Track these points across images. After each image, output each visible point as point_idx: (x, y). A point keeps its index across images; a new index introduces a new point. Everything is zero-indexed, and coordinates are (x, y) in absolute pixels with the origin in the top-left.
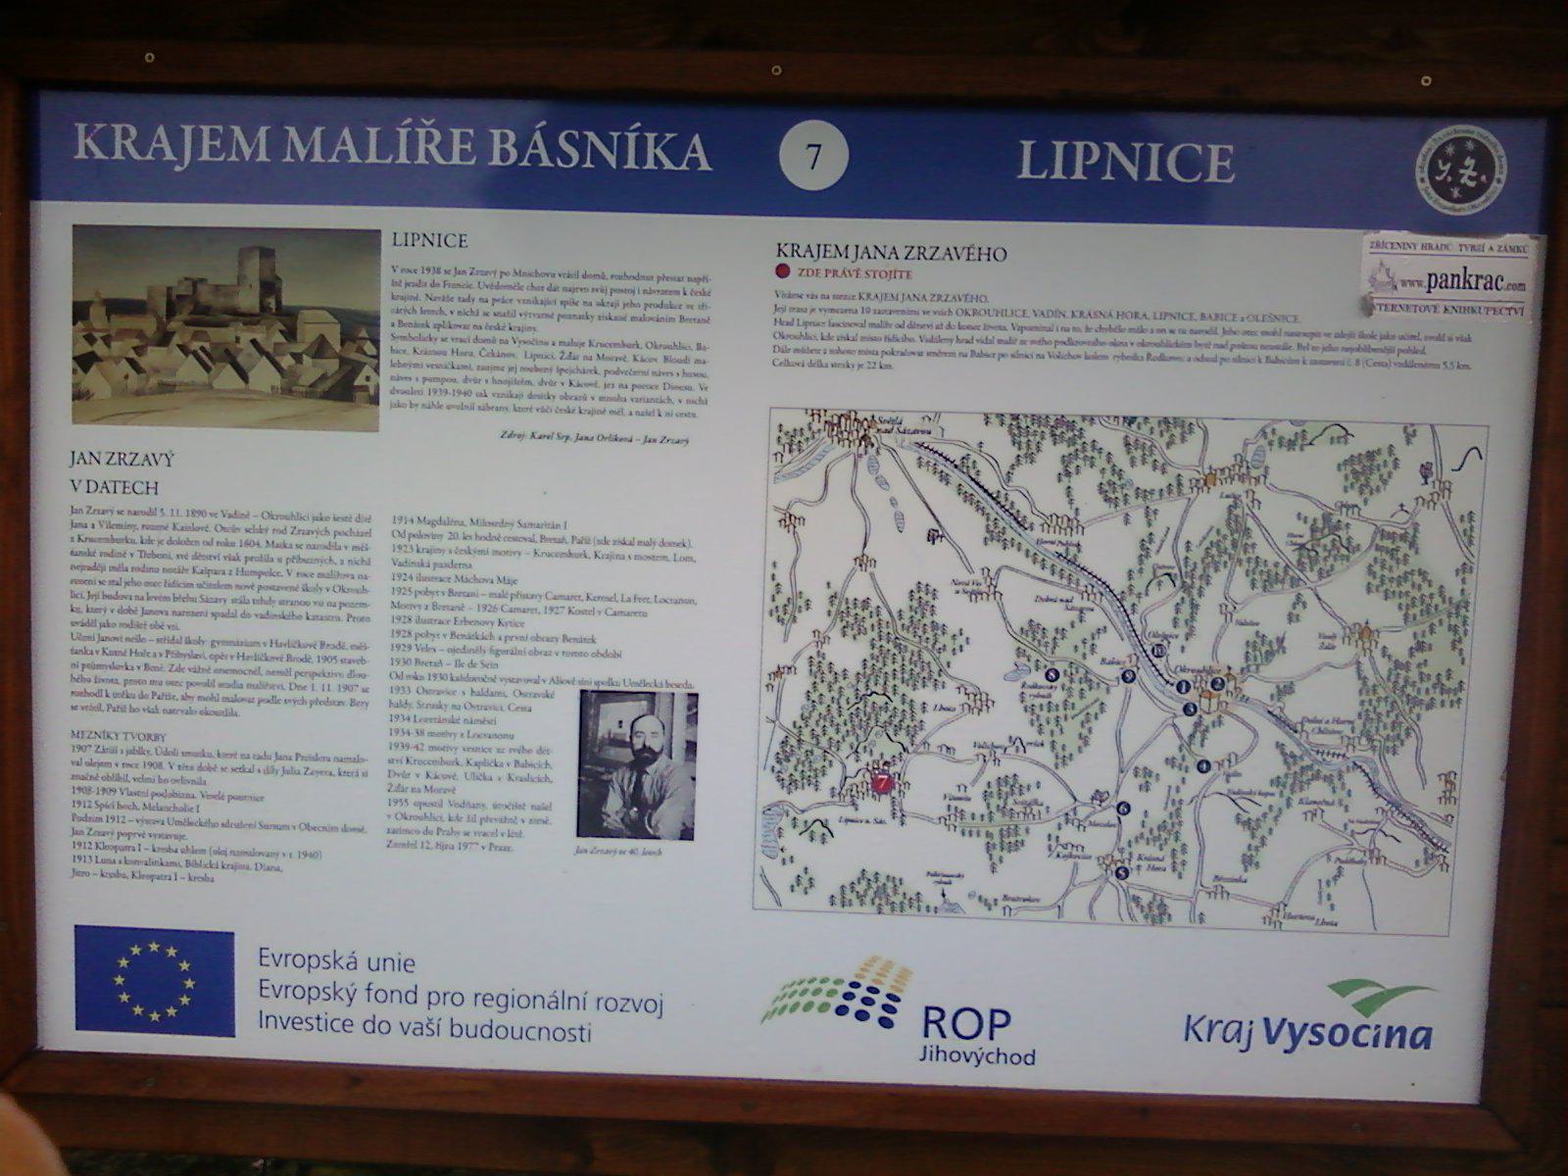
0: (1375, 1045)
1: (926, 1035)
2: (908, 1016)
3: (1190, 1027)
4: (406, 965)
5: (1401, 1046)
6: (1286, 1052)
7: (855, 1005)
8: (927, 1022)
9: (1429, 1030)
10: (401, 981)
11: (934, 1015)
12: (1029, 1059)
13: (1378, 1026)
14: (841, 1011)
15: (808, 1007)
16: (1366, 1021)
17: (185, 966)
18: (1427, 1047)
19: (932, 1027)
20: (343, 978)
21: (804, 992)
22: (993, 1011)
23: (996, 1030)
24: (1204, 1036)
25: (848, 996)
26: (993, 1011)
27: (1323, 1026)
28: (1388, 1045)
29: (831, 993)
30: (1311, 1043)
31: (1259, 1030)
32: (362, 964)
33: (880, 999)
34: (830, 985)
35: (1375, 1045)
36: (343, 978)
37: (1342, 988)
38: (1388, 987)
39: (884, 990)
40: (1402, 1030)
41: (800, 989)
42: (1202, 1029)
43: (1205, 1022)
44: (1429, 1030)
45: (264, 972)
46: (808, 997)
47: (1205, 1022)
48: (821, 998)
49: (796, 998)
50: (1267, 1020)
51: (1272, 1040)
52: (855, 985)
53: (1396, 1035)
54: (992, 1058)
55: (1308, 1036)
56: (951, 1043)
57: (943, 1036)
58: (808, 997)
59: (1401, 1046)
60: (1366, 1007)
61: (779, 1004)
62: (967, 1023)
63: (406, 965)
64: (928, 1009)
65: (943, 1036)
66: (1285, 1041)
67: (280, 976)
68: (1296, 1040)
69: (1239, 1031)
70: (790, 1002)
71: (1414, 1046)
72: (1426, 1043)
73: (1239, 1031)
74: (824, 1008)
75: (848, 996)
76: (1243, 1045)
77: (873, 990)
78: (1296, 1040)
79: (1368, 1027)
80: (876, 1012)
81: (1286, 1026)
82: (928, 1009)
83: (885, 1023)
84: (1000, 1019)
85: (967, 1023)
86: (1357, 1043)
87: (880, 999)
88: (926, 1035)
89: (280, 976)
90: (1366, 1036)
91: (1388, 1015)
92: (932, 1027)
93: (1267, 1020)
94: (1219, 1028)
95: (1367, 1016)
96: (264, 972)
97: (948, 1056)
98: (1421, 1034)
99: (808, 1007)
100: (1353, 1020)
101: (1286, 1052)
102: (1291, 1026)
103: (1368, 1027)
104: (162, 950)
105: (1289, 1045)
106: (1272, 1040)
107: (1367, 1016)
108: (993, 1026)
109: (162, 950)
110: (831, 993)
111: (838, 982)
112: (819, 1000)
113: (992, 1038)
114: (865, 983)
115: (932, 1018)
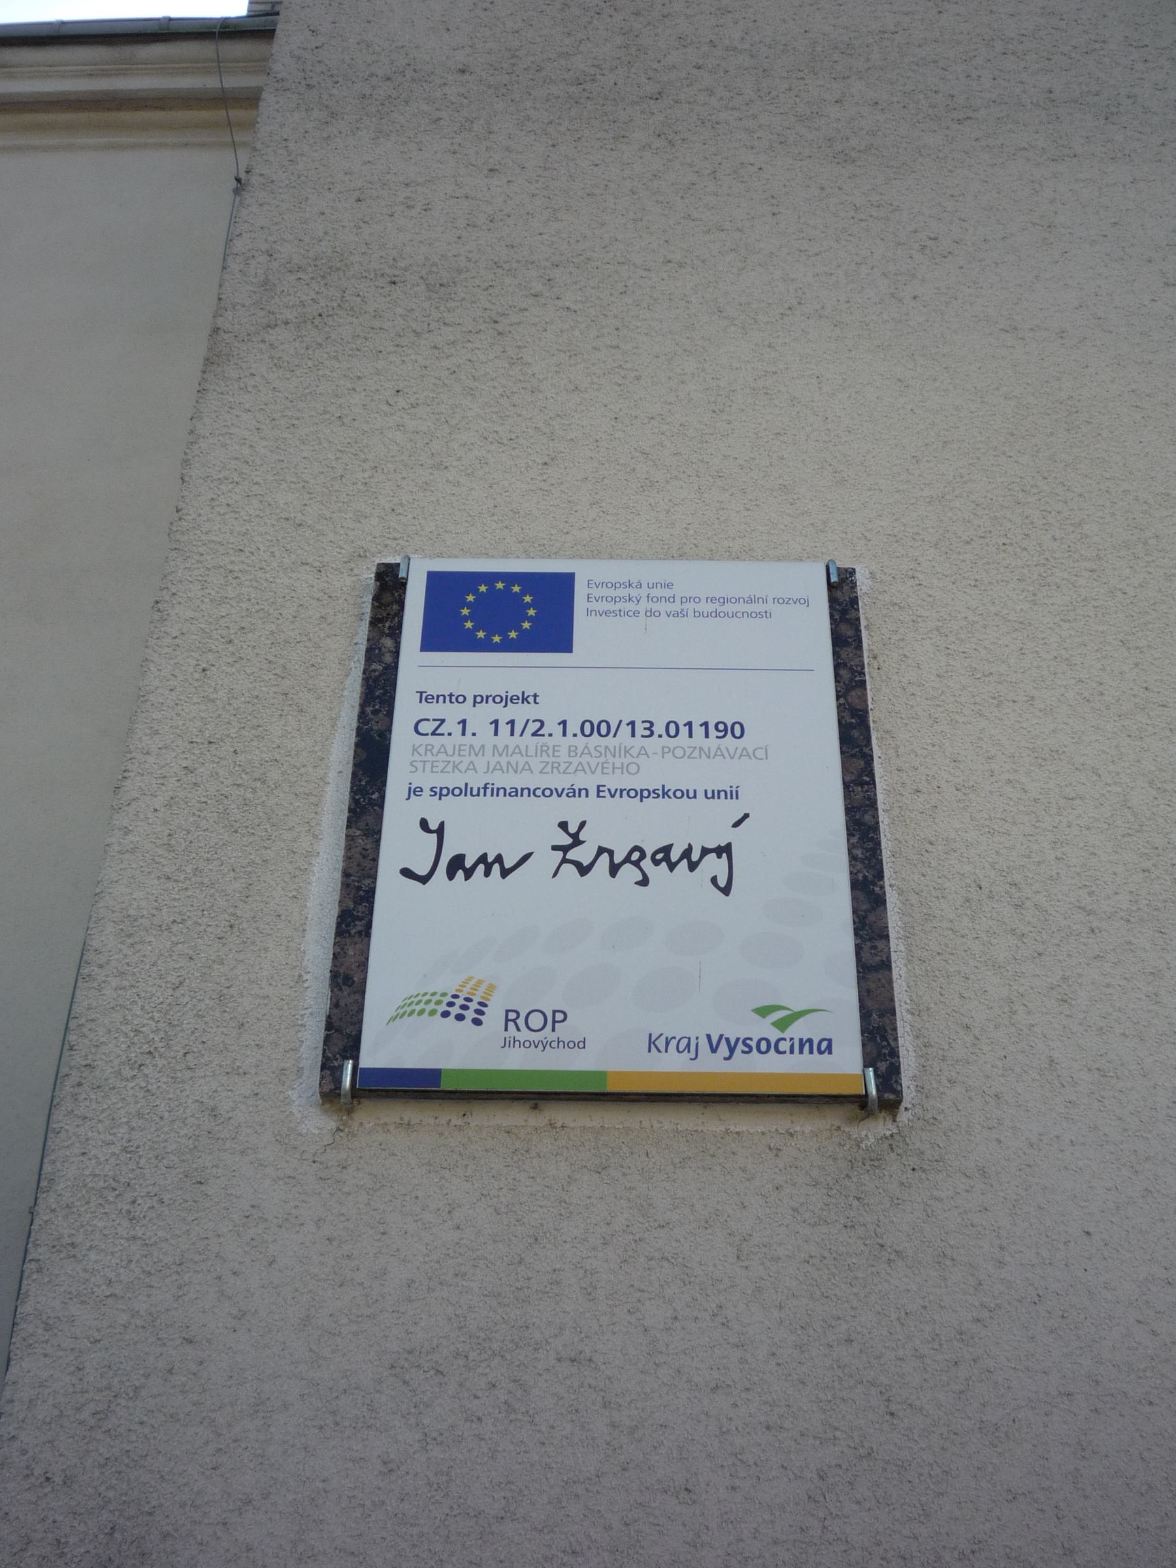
0: (792, 1052)
1: (506, 1029)
2: (494, 1017)
3: (652, 1043)
4: (669, 585)
5: (811, 1052)
6: (725, 1059)
7: (455, 1010)
8: (507, 1020)
9: (830, 1041)
10: (667, 593)
11: (512, 1016)
12: (582, 1044)
13: (791, 1039)
14: (446, 1014)
15: (422, 1012)
16: (782, 1036)
17: (481, 634)
18: (830, 1053)
19: (511, 1024)
20: (634, 592)
21: (419, 1002)
22: (554, 1012)
23: (557, 1025)
24: (663, 1049)
25: (451, 1004)
26: (554, 1012)
27: (751, 1039)
28: (801, 1052)
29: (439, 1003)
30: (743, 1052)
31: (704, 1042)
32: (644, 585)
33: (473, 1006)
34: (437, 997)
35: (792, 1052)
36: (634, 592)
37: (763, 1012)
38: (796, 1010)
39: (476, 999)
40: (810, 1041)
41: (416, 1000)
42: (661, 1044)
43: (663, 1039)
44: (830, 1041)
45: (590, 591)
46: (422, 1006)
47: (663, 1039)
48: (432, 1006)
49: (413, 1007)
50: (709, 1037)
51: (714, 1050)
52: (455, 996)
53: (805, 1044)
54: (554, 1044)
55: (740, 1046)
56: (524, 1035)
57: (518, 1030)
58: (422, 1006)
59: (811, 1052)
60: (782, 1025)
61: (401, 1011)
62: (536, 1021)
63: (669, 585)
64: (507, 1011)
65: (518, 1030)
66: (723, 1050)
67: (597, 592)
68: (732, 1050)
69: (688, 1045)
70: (409, 1010)
71: (821, 1052)
72: (829, 1049)
73: (688, 1045)
74: (432, 1013)
75: (451, 1004)
76: (693, 1055)
77: (468, 1000)
78: (732, 1050)
79: (784, 1039)
80: (470, 1015)
81: (723, 1041)
82: (507, 1011)
83: (477, 1022)
84: (559, 1017)
85: (536, 1021)
86: (778, 1051)
87: (473, 1006)
88: (506, 1029)
89: (597, 592)
90: (784, 1046)
91: (798, 1031)
92: (511, 1024)
93: (709, 1037)
94: (673, 1043)
95: (783, 1031)
96: (590, 591)
97: (522, 1044)
98: (824, 1045)
99: (422, 1012)
100: (774, 1035)
101: (725, 1059)
102: (728, 1040)
103: (784, 1039)
104: (507, 588)
105: (727, 1054)
106: (714, 1050)
107: (783, 1031)
108: (554, 1022)
109: (507, 588)
110: (439, 1003)
111: (444, 995)
112: (429, 1008)
113: (553, 1030)
114: (462, 995)
115: (511, 1018)
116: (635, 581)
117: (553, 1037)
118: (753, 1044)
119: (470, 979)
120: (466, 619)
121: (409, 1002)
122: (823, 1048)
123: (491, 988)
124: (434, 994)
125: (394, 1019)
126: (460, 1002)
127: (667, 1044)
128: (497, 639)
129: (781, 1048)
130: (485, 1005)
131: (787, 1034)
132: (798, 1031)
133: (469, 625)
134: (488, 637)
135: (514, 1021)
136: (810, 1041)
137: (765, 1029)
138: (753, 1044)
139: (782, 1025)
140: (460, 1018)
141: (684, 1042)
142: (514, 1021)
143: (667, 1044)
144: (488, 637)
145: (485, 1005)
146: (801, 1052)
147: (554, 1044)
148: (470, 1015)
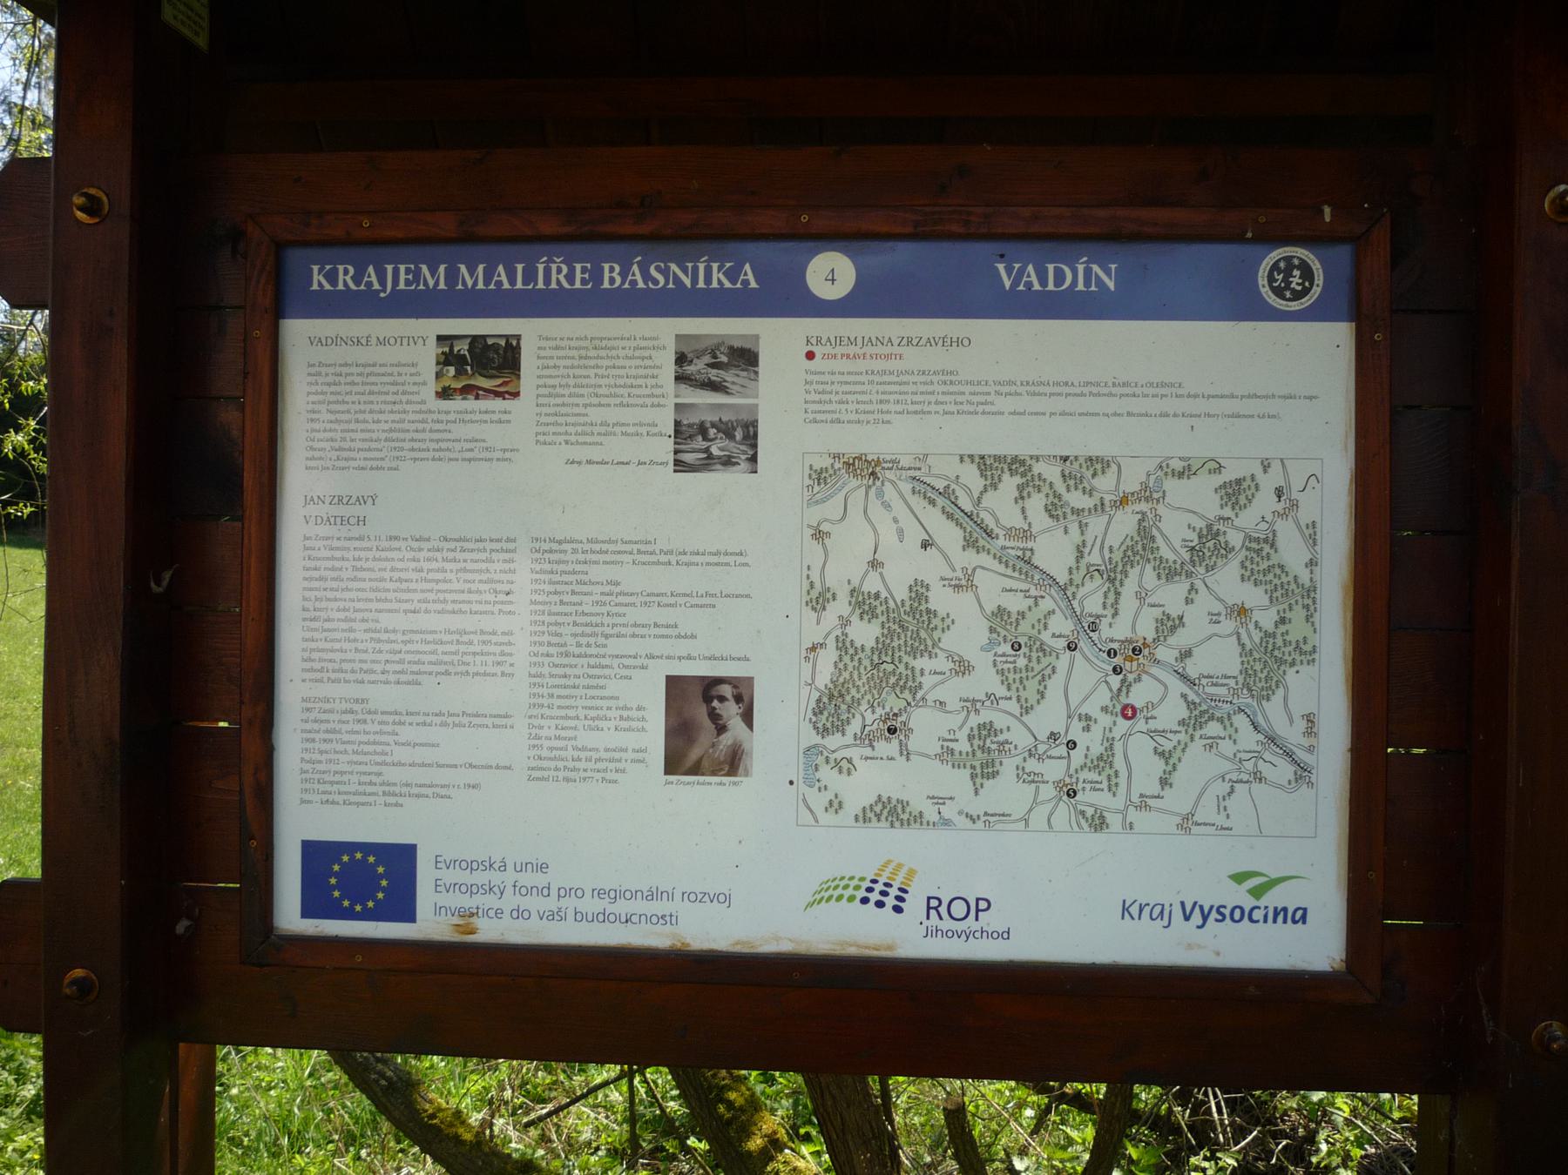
0: (1265, 921)
3: (1125, 909)
7: (875, 896)
8: (929, 908)
9: (1305, 910)
11: (934, 903)
14: (865, 901)
15: (839, 898)
16: (1256, 903)
17: (346, 903)
19: (933, 912)
21: (836, 887)
22: (978, 900)
24: (1136, 916)
25: (870, 890)
26: (978, 900)
28: (1275, 921)
29: (857, 888)
32: (510, 867)
33: (894, 892)
34: (855, 882)
35: (1265, 921)
36: (495, 877)
37: (1239, 878)
39: (896, 885)
40: (1285, 910)
42: (1134, 910)
44: (1305, 910)
45: (439, 873)
48: (850, 892)
49: (830, 892)
50: (1183, 904)
51: (1187, 918)
52: (874, 881)
54: (978, 935)
55: (1214, 915)
56: (947, 924)
59: (1285, 921)
60: (1257, 892)
61: (818, 897)
62: (959, 909)
64: (929, 899)
66: (1197, 918)
67: (450, 876)
68: (1205, 918)
69: (1162, 912)
70: (826, 895)
72: (1304, 919)
73: (1162, 912)
74: (851, 899)
75: (870, 890)
76: (1166, 922)
78: (1205, 918)
80: (890, 901)
81: (1197, 909)
82: (929, 899)
83: (898, 910)
84: (983, 905)
85: (959, 909)
87: (894, 892)
89: (450, 876)
90: (1257, 915)
91: (1273, 899)
92: (933, 912)
93: (1183, 904)
94: (1147, 910)
95: (1258, 898)
97: (945, 934)
99: (839, 898)
100: (1248, 902)
102: (1201, 908)
105: (1200, 922)
106: (1187, 918)
107: (1258, 898)
108: (978, 910)
110: (857, 888)
112: (847, 893)
116: (497, 858)
117: (975, 926)
118: (1227, 912)
119: (889, 862)
120: (333, 888)
121: (826, 886)
122: (1298, 916)
123: (911, 873)
124: (852, 878)
125: (811, 905)
126: (879, 887)
127: (1141, 911)
128: (358, 908)
129: (1255, 917)
130: (905, 891)
131: (1262, 902)
132: (1273, 899)
133: (336, 894)
134: (352, 906)
135: (936, 908)
136: (1285, 910)
137: (1239, 896)
138: (1227, 912)
139: (1257, 892)
140: (880, 904)
141: (1157, 910)
142: (936, 908)
143: (1141, 911)
144: (352, 906)
145: (905, 891)
146: (1275, 921)
147: (978, 935)
148: (890, 901)
